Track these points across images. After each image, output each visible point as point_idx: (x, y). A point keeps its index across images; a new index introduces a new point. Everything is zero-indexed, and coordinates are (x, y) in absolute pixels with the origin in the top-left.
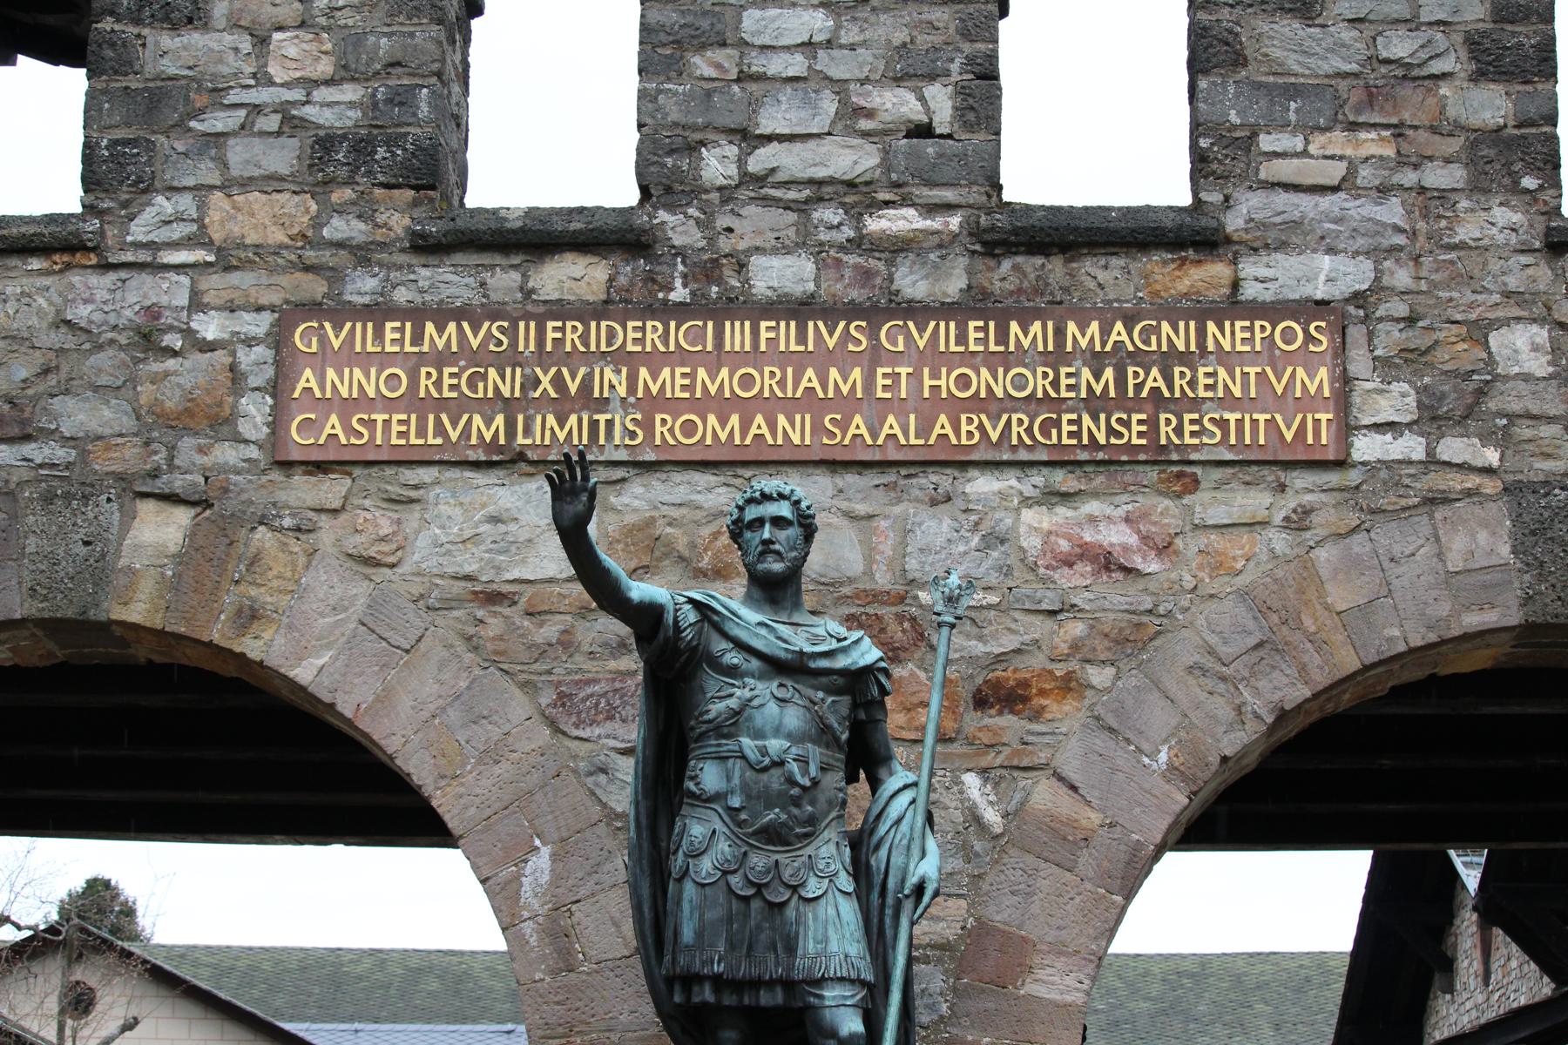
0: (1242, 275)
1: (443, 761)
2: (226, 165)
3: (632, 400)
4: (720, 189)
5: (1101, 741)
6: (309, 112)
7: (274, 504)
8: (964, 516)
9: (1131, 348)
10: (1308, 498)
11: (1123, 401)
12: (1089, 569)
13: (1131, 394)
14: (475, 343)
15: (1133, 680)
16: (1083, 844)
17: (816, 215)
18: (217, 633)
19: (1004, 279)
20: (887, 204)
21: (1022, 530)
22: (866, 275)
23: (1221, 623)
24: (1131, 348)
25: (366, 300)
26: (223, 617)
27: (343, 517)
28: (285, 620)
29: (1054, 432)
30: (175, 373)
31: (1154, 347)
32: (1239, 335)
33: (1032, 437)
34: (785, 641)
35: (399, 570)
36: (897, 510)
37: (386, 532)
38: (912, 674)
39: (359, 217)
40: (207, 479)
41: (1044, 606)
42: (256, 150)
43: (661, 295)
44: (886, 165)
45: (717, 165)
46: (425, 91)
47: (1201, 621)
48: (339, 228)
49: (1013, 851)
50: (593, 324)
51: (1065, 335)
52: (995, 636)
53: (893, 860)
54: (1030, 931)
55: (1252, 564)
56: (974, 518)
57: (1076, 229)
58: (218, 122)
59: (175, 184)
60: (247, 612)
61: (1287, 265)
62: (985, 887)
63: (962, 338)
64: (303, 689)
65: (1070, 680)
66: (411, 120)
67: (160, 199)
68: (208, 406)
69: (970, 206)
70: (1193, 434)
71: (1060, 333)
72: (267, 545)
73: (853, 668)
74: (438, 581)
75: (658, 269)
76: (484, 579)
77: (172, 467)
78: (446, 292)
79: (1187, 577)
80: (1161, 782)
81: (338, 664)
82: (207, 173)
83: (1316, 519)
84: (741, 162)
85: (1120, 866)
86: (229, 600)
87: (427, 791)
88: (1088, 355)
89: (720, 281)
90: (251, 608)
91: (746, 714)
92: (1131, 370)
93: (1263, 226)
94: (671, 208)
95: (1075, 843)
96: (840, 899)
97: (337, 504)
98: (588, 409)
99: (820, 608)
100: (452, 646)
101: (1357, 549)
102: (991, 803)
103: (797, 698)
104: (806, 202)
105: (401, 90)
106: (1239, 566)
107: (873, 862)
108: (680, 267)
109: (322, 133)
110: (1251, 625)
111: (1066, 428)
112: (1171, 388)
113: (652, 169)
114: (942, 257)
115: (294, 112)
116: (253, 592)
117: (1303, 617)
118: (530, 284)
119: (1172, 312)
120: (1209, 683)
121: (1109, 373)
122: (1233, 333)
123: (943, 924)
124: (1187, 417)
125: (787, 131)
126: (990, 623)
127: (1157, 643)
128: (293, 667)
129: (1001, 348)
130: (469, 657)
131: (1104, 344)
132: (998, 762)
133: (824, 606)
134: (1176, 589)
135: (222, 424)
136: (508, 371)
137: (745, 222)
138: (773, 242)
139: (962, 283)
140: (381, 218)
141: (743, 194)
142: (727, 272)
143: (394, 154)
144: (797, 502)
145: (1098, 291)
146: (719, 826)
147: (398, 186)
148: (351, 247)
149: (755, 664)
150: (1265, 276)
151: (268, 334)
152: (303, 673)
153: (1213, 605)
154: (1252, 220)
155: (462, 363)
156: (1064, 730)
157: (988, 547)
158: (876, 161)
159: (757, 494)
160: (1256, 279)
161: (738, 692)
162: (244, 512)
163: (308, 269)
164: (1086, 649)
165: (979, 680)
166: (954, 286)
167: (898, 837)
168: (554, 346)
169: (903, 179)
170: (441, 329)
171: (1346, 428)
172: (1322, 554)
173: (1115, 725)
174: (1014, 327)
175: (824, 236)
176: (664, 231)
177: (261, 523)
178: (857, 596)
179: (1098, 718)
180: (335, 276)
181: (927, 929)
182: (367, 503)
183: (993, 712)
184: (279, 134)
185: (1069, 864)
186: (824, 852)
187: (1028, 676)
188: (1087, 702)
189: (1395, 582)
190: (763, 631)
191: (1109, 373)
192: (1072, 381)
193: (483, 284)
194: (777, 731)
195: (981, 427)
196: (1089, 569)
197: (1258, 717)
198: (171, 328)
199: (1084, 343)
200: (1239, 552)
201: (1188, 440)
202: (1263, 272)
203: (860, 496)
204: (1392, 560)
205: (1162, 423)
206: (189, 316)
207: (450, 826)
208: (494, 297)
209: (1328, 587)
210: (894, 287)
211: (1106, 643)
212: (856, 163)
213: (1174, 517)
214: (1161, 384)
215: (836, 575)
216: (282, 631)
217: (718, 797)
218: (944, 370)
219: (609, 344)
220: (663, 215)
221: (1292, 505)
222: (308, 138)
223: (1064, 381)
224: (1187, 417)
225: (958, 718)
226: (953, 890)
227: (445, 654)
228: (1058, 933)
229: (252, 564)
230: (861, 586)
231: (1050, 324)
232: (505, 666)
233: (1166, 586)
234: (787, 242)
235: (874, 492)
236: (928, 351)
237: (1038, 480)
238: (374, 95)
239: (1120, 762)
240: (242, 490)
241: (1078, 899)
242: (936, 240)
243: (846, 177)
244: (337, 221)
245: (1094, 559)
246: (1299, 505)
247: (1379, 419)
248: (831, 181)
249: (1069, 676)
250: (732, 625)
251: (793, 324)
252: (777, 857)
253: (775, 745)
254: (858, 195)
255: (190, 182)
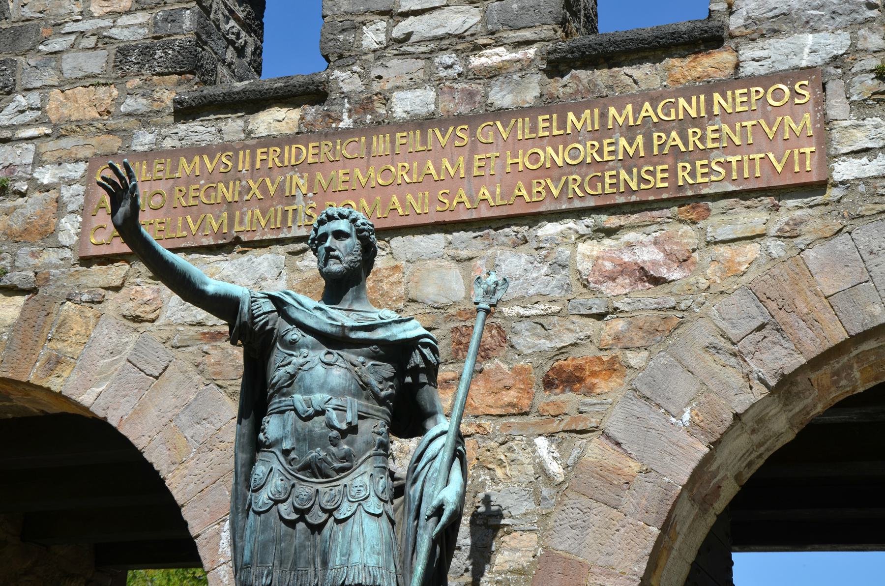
0: (742, 58)
1: (174, 452)
2: (61, 72)
3: (310, 195)
4: (374, 51)
5: (639, 407)
6: (114, 32)
7: (78, 286)
8: (537, 252)
9: (655, 120)
10: (799, 213)
11: (650, 157)
12: (627, 281)
13: (656, 152)
14: (210, 167)
15: (663, 359)
16: (625, 486)
17: (437, 60)
18: (33, 376)
19: (565, 86)
20: (485, 46)
21: (578, 258)
22: (471, 95)
23: (738, 314)
24: (655, 120)
25: (146, 148)
26: (38, 364)
27: (123, 291)
28: (78, 363)
29: (599, 185)
30: (21, 206)
31: (673, 117)
32: (739, 100)
33: (584, 191)
34: (334, 320)
35: (156, 323)
36: (489, 252)
37: (149, 298)
38: (498, 367)
39: (143, 96)
40: (36, 273)
41: (594, 311)
42: (80, 60)
43: (334, 125)
44: (485, 21)
45: (373, 36)
46: (188, 12)
47: (714, 311)
48: (131, 104)
49: (571, 494)
50: (287, 148)
51: (607, 117)
52: (558, 335)
53: (425, 490)
54: (586, 557)
55: (754, 266)
56: (544, 252)
57: (615, 42)
58: (57, 44)
59: (29, 86)
60: (54, 359)
61: (777, 45)
62: (551, 523)
63: (534, 129)
64: (87, 409)
65: (614, 363)
66: (179, 31)
67: (19, 97)
68: (41, 226)
69: (542, 40)
70: (703, 175)
71: (603, 116)
72: (71, 313)
73: (391, 339)
74: (180, 328)
75: (333, 108)
76: (210, 324)
77: (14, 267)
78: (195, 138)
79: (703, 280)
80: (686, 436)
81: (111, 390)
82: (49, 77)
83: (804, 228)
84: (388, 32)
85: (656, 503)
86: (43, 354)
87: (163, 474)
88: (624, 129)
89: (372, 111)
90: (57, 357)
91: (298, 376)
92: (655, 135)
93: (756, 21)
94: (341, 68)
95: (619, 486)
96: (367, 519)
97: (118, 283)
98: (281, 203)
99: (434, 326)
100: (186, 371)
101: (840, 248)
102: (554, 458)
103: (340, 362)
104: (431, 52)
105: (172, 12)
106: (743, 268)
107: (411, 493)
108: (347, 105)
109: (121, 45)
110: (754, 311)
111: (608, 181)
112: (686, 144)
113: (330, 44)
114: (522, 77)
115: (105, 34)
116: (59, 345)
117: (797, 302)
118: (250, 128)
119: (687, 93)
120: (722, 358)
121: (640, 139)
122: (734, 99)
123: (519, 554)
124: (699, 163)
125: (418, 7)
126: (555, 326)
127: (678, 331)
128: (80, 394)
129: (562, 132)
130: (197, 378)
131: (635, 120)
132: (562, 427)
133: (437, 323)
134: (693, 290)
135: (47, 235)
136: (231, 184)
137: (390, 71)
138: (408, 81)
139: (536, 93)
140: (156, 96)
141: (390, 52)
142: (377, 105)
143: (166, 53)
144: (354, 221)
145: (634, 85)
146: (276, 466)
147: (170, 74)
148: (138, 115)
149: (309, 338)
150: (758, 57)
151: (82, 177)
152: (86, 399)
153: (723, 299)
154: (750, 18)
155: (202, 182)
156: (610, 400)
157: (554, 273)
158: (479, 18)
159: (324, 216)
160: (754, 60)
161: (294, 360)
162: (58, 293)
163: (109, 132)
164: (625, 340)
165: (547, 368)
166: (530, 94)
167: (432, 471)
168: (261, 165)
169: (496, 27)
170: (189, 162)
171: (827, 157)
172: (810, 254)
173: (648, 395)
174: (571, 116)
175: (443, 73)
176: (337, 84)
177: (69, 300)
178: (460, 314)
179: (635, 390)
180: (127, 135)
181: (507, 558)
182: (139, 280)
183: (558, 391)
184: (95, 48)
185: (614, 503)
186: (358, 482)
187: (583, 362)
188: (627, 379)
189: (875, 269)
190: (318, 313)
191: (640, 139)
192: (612, 148)
193: (220, 131)
194: (322, 387)
195: (547, 188)
196: (627, 281)
197: (762, 381)
198: (21, 178)
199: (620, 121)
200: (744, 259)
201: (700, 180)
202: (758, 53)
203: (463, 245)
204: (871, 253)
205: (680, 169)
206: (33, 170)
207: (176, 498)
208: (226, 138)
209: (818, 278)
210: (489, 102)
211: (641, 334)
212: (464, 22)
213: (690, 237)
214: (679, 142)
215: (445, 301)
216: (76, 370)
217: (278, 442)
218: (521, 152)
219: (297, 159)
220: (337, 73)
221: (785, 220)
222: (112, 49)
223: (606, 149)
224: (699, 163)
225: (532, 397)
226: (527, 527)
227: (182, 377)
228: (607, 558)
229: (60, 327)
230: (463, 307)
231: (596, 111)
232: (219, 383)
233: (686, 288)
234: (418, 80)
235: (474, 241)
236: (510, 140)
237: (589, 221)
238: (155, 18)
239: (653, 422)
240: (58, 279)
241: (622, 530)
242: (519, 65)
243: (457, 33)
244: (130, 101)
245: (631, 274)
246: (791, 219)
247: (855, 148)
248: (449, 36)
249: (613, 360)
250: (293, 309)
251: (418, 132)
252: (319, 487)
253: (318, 398)
254: (466, 43)
255: (38, 84)
